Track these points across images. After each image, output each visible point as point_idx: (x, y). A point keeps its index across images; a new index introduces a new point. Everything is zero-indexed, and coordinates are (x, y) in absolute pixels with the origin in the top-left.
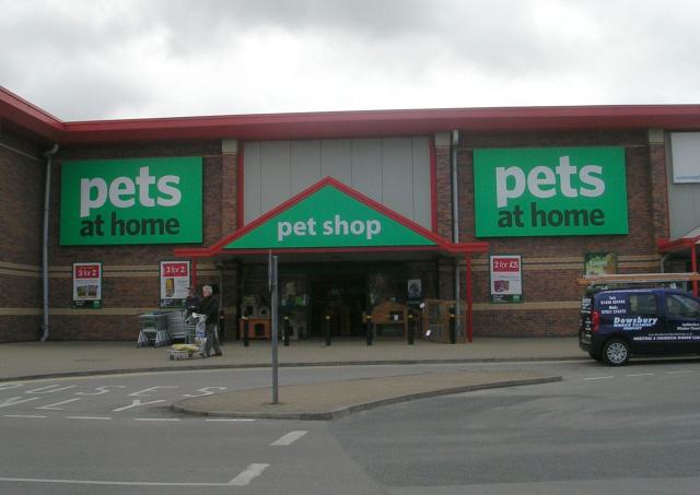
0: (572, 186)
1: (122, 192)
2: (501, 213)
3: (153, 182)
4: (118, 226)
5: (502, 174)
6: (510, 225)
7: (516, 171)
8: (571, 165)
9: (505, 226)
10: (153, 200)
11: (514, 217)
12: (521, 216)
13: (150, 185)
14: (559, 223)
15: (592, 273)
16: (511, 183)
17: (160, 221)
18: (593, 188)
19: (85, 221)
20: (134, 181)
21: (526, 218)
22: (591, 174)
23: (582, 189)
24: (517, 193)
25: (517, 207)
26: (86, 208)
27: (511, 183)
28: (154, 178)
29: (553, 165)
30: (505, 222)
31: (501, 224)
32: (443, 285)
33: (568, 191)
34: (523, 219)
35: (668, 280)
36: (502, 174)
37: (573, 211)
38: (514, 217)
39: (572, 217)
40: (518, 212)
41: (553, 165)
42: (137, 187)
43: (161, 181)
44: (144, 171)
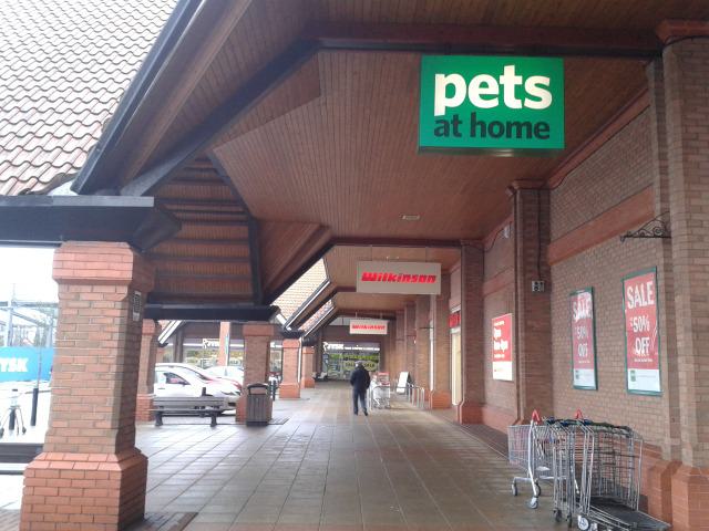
0: (517, 97)
1: (484, 91)
2: (438, 122)
3: (521, 83)
4: (478, 128)
5: (441, 81)
6: (446, 134)
7: (457, 79)
8: (516, 74)
9: (441, 135)
10: (520, 101)
11: (451, 127)
12: (460, 126)
13: (516, 86)
14: (501, 133)
15: (169, 377)
16: (450, 92)
17: (528, 124)
18: (539, 99)
19: (440, 120)
20: (498, 80)
21: (465, 128)
22: (538, 85)
23: (527, 100)
24: (456, 101)
25: (456, 117)
26: (441, 105)
27: (450, 92)
28: (520, 78)
29: (497, 73)
30: (442, 131)
31: (437, 133)
32: (577, 377)
33: (512, 102)
34: (460, 128)
35: (85, 486)
36: (441, 81)
37: (517, 124)
38: (451, 127)
39: (514, 129)
40: (456, 121)
41: (497, 73)
42: (501, 87)
43: (528, 81)
44: (509, 70)
